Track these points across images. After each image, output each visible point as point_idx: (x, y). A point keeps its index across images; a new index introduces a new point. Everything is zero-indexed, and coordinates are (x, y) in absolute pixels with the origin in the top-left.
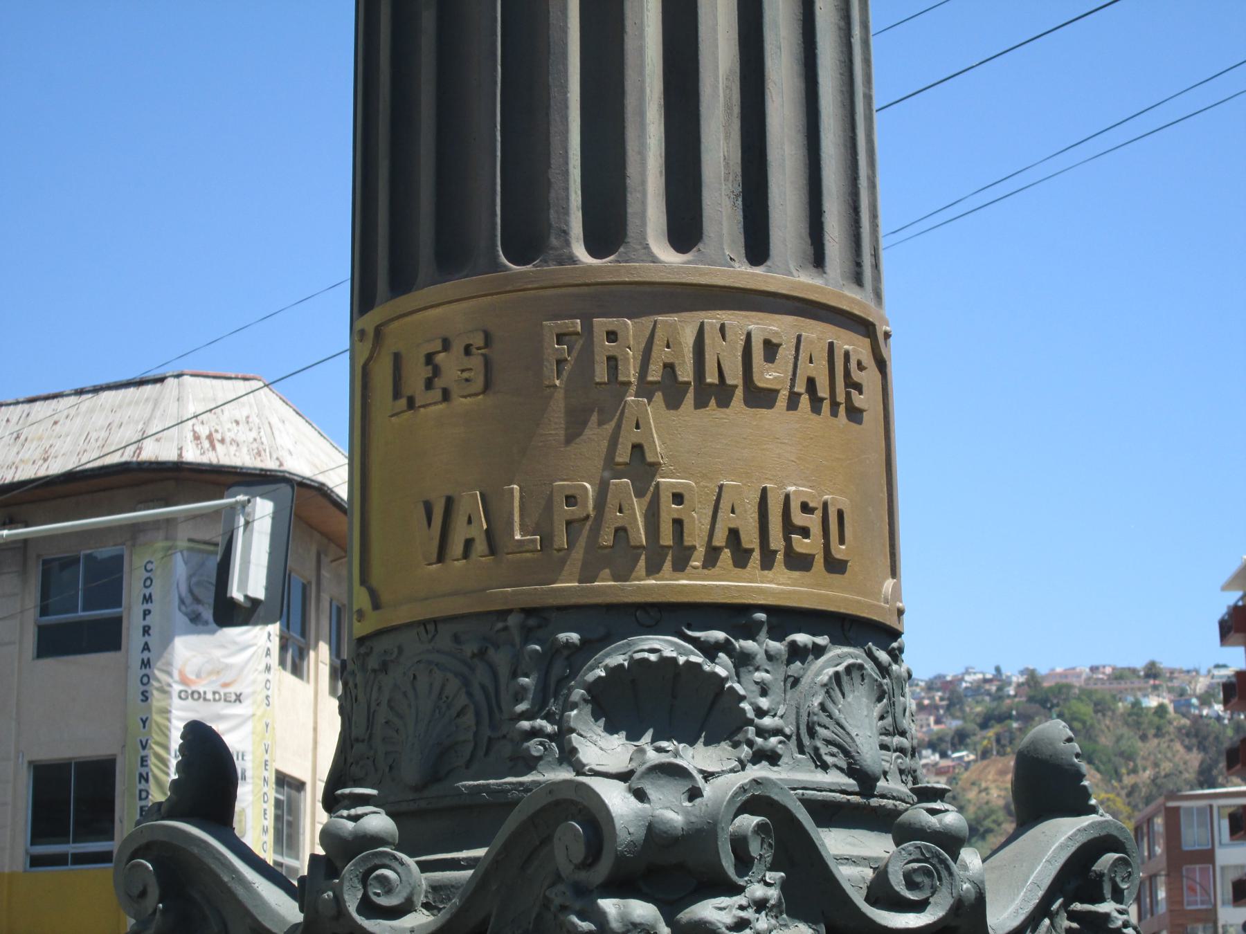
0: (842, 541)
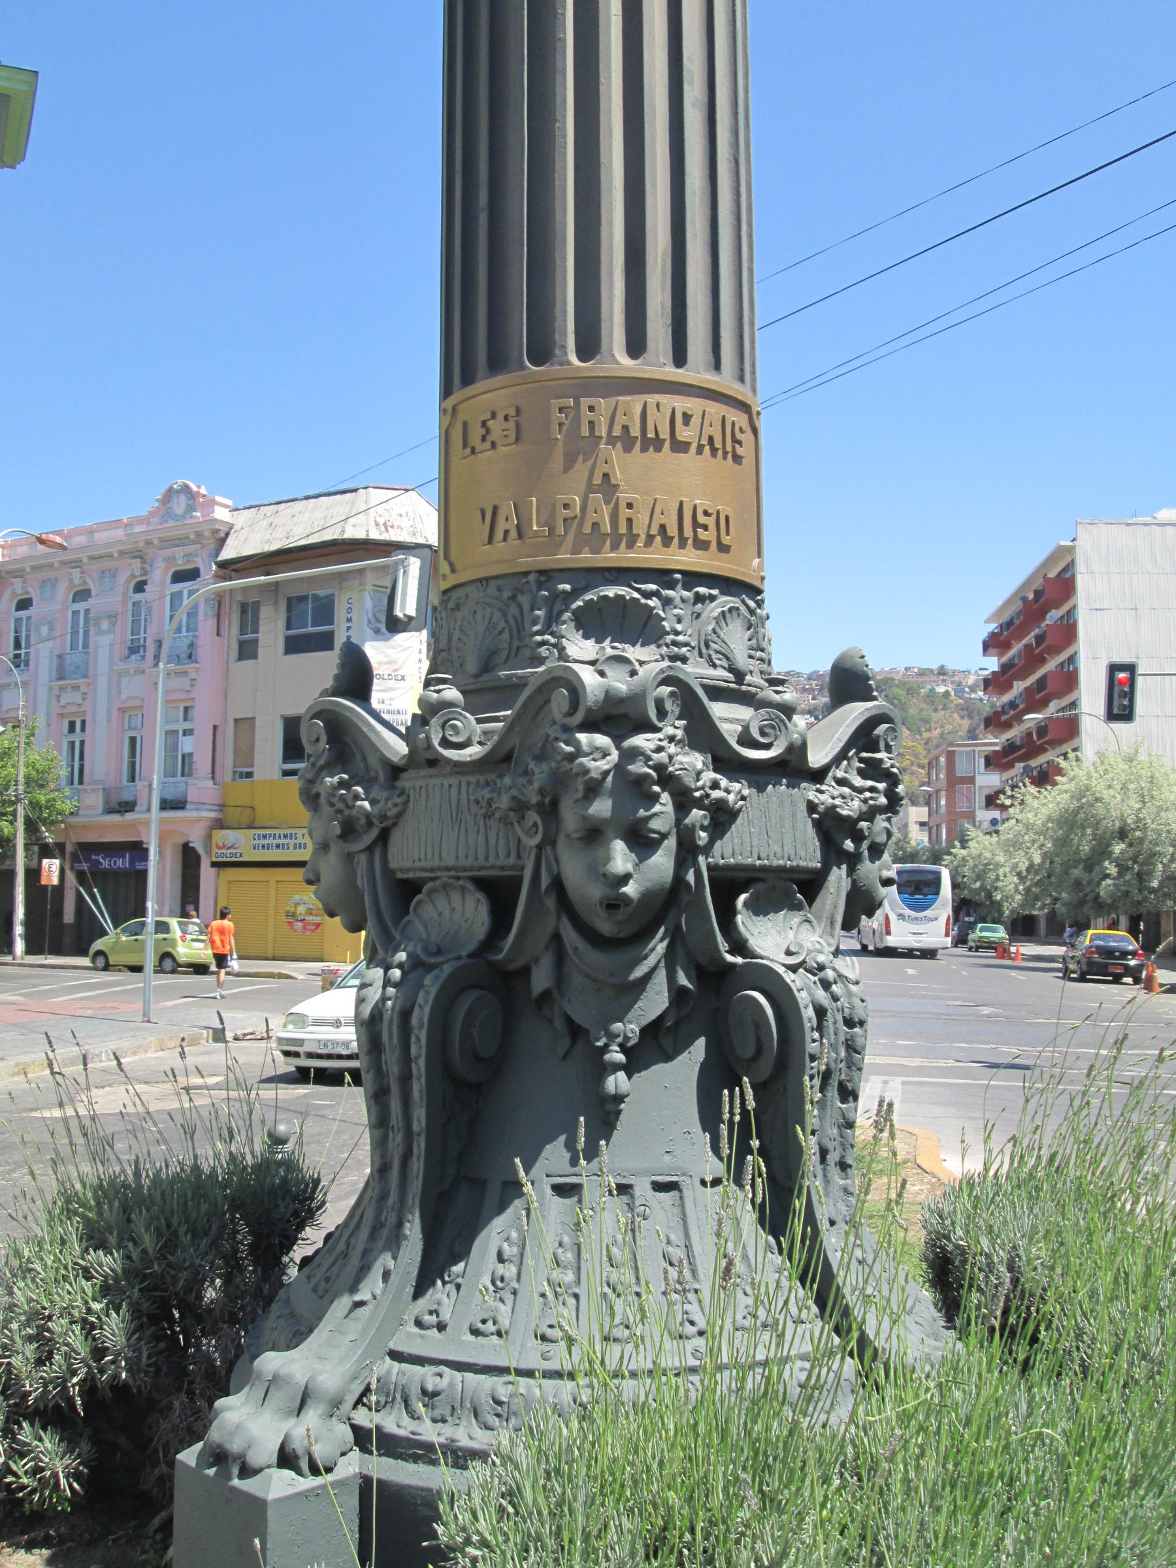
0: (728, 534)
